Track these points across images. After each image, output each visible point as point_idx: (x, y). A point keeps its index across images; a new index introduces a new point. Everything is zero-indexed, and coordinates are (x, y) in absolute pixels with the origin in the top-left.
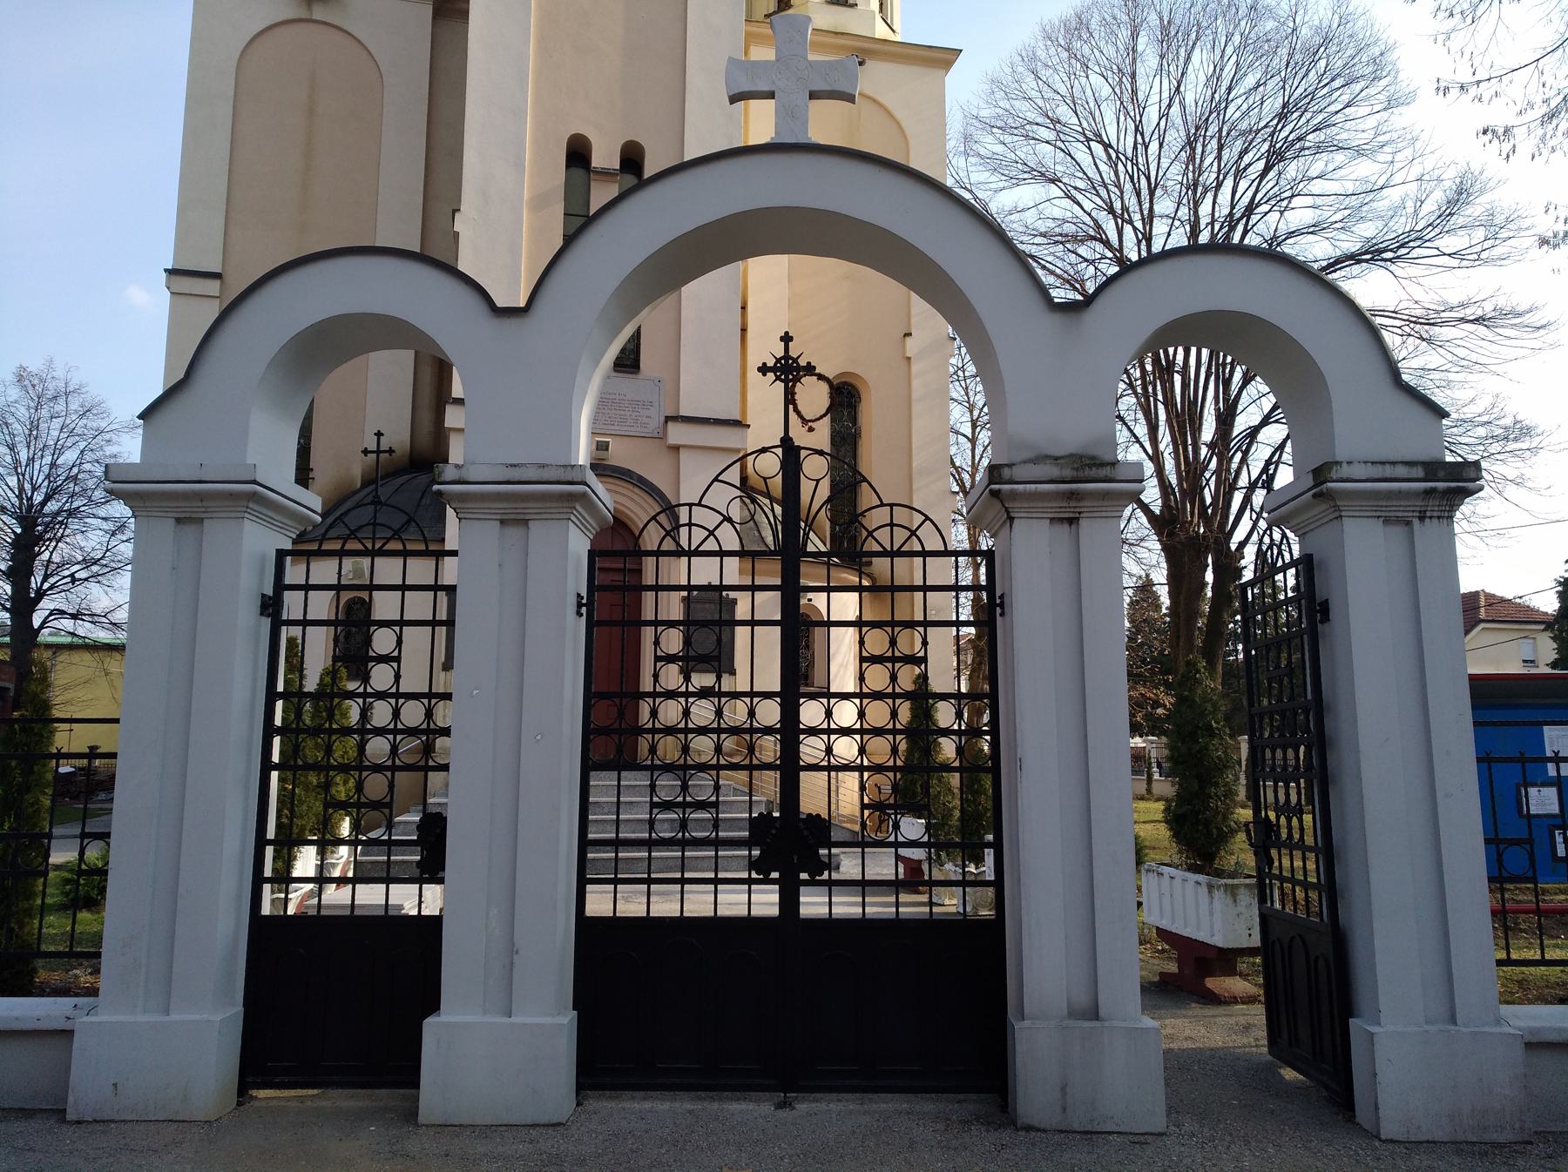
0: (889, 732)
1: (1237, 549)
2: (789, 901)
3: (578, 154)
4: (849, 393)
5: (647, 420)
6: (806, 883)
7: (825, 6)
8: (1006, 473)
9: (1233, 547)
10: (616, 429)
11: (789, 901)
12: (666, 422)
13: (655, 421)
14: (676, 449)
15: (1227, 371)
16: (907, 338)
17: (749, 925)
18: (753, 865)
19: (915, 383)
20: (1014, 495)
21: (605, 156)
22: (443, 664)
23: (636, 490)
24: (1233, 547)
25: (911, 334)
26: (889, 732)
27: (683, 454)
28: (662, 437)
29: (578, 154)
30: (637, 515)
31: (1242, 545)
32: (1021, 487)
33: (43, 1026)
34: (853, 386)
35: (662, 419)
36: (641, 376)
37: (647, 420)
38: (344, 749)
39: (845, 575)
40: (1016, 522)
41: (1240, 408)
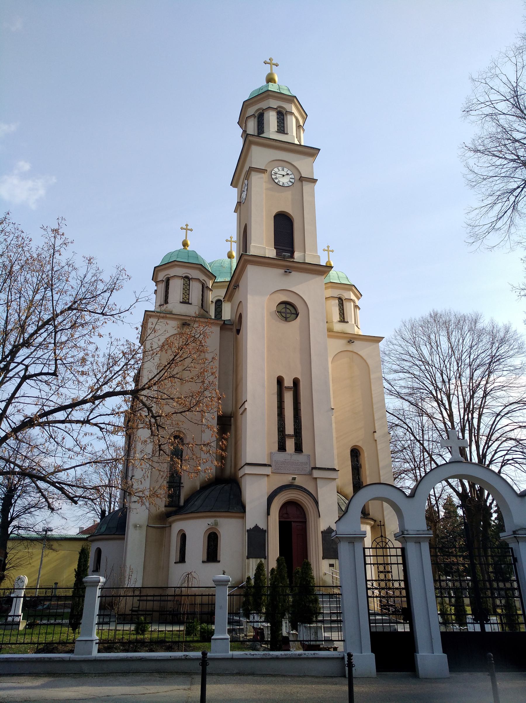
0: (385, 580)
1: (489, 505)
2: (483, 628)
3: (280, 381)
4: (356, 452)
5: (306, 469)
6: (485, 624)
7: (339, 323)
8: (517, 532)
9: (488, 505)
10: (296, 472)
11: (483, 628)
12: (312, 469)
13: (308, 469)
14: (316, 479)
15: (476, 438)
16: (375, 433)
17: (475, 633)
18: (474, 619)
19: (379, 447)
20: (519, 537)
21: (288, 383)
22: (247, 556)
23: (305, 493)
24: (488, 505)
25: (376, 432)
26: (385, 580)
27: (318, 480)
28: (311, 474)
29: (280, 381)
30: (305, 502)
31: (491, 504)
32: (520, 536)
33: (329, 657)
34: (357, 450)
35: (311, 468)
36: (303, 454)
37: (306, 469)
38: (383, 593)
39: (370, 521)
40: (519, 543)
41: (487, 454)
